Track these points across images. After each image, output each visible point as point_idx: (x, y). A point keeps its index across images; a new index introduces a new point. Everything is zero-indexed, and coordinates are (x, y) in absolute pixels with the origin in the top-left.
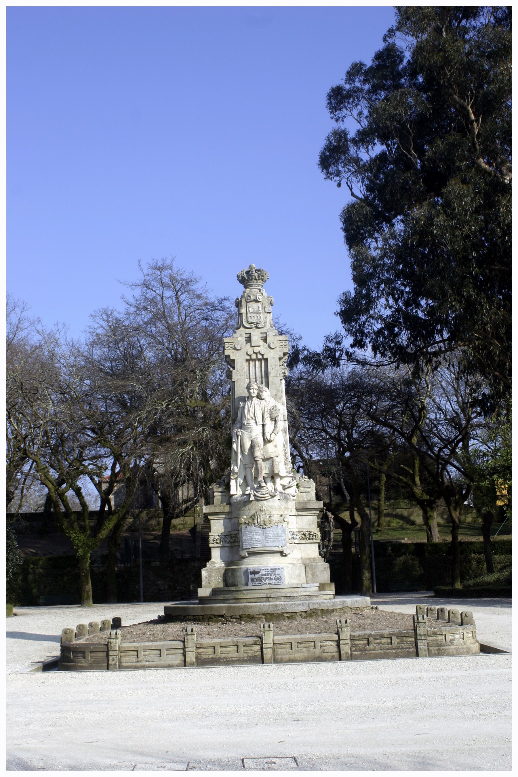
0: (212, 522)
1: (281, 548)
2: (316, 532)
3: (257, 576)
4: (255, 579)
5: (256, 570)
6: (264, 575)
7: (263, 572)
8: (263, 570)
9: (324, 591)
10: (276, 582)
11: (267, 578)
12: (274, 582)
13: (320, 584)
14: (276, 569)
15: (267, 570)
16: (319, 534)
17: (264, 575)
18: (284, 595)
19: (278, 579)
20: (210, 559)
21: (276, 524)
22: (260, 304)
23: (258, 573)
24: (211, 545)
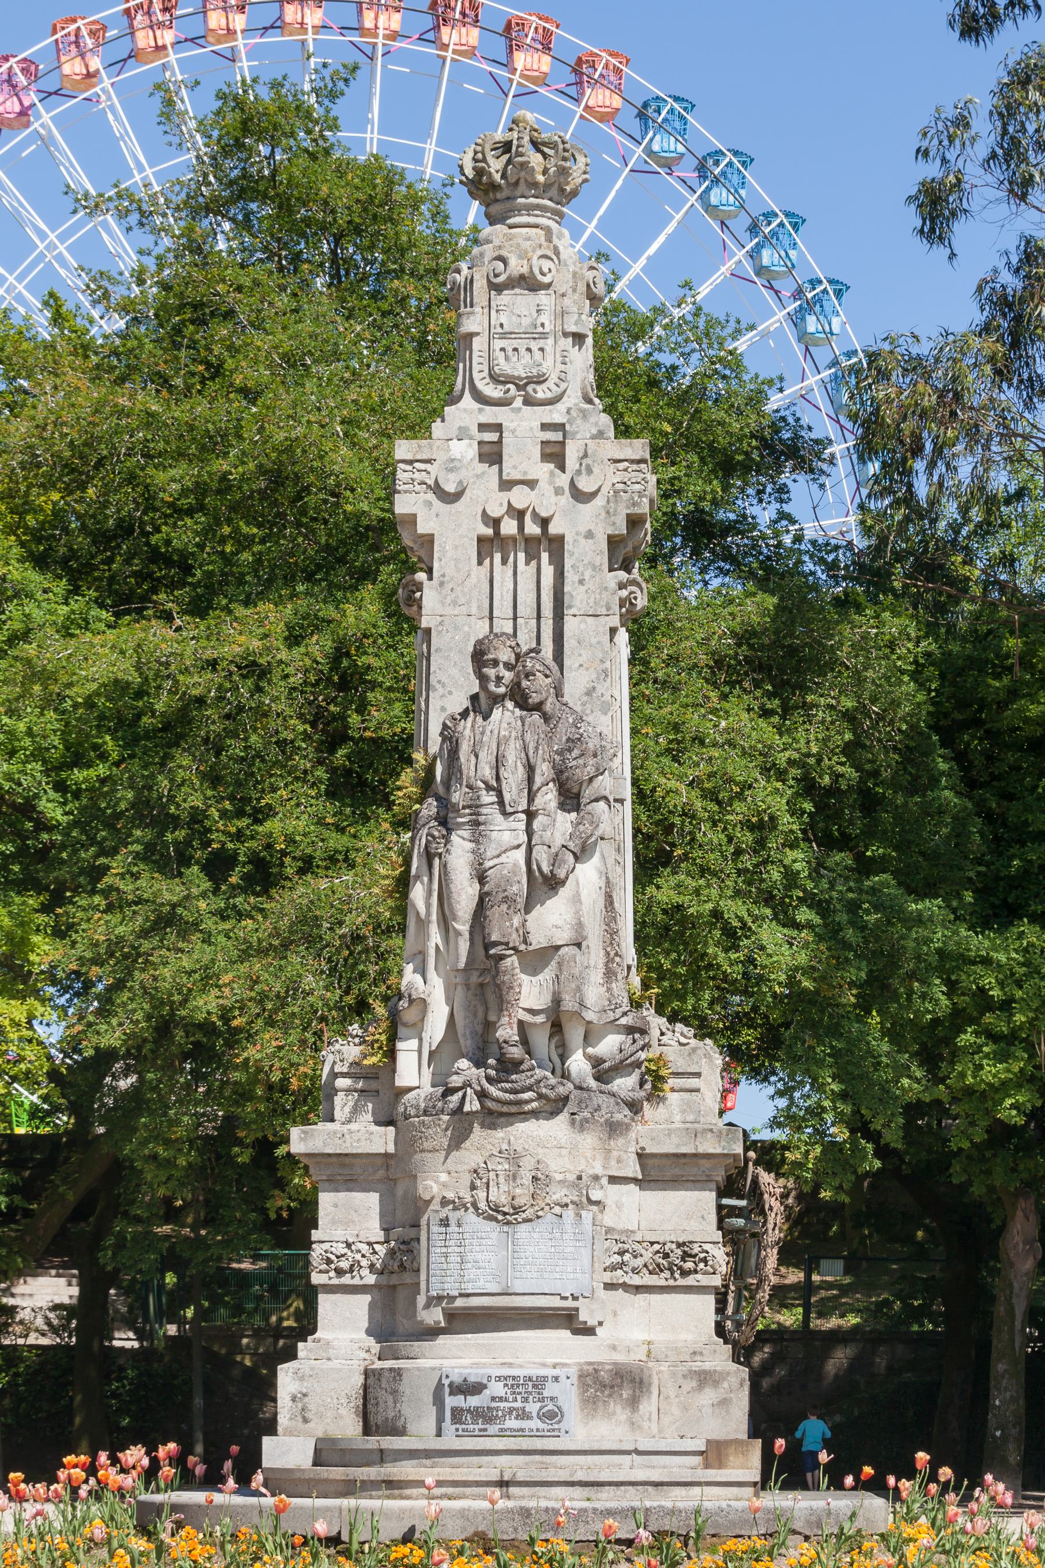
0: (326, 1200)
1: (569, 1303)
2: (706, 1247)
3: (473, 1401)
4: (469, 1411)
5: (472, 1379)
6: (501, 1399)
7: (497, 1389)
8: (499, 1379)
9: (720, 1468)
10: (540, 1425)
11: (511, 1410)
12: (535, 1424)
13: (708, 1441)
14: (545, 1378)
15: (513, 1383)
16: (720, 1255)
17: (501, 1399)
18: (563, 1476)
19: (551, 1416)
20: (314, 1331)
21: (557, 1210)
22: (543, 298)
23: (476, 1388)
24: (316, 1279)
